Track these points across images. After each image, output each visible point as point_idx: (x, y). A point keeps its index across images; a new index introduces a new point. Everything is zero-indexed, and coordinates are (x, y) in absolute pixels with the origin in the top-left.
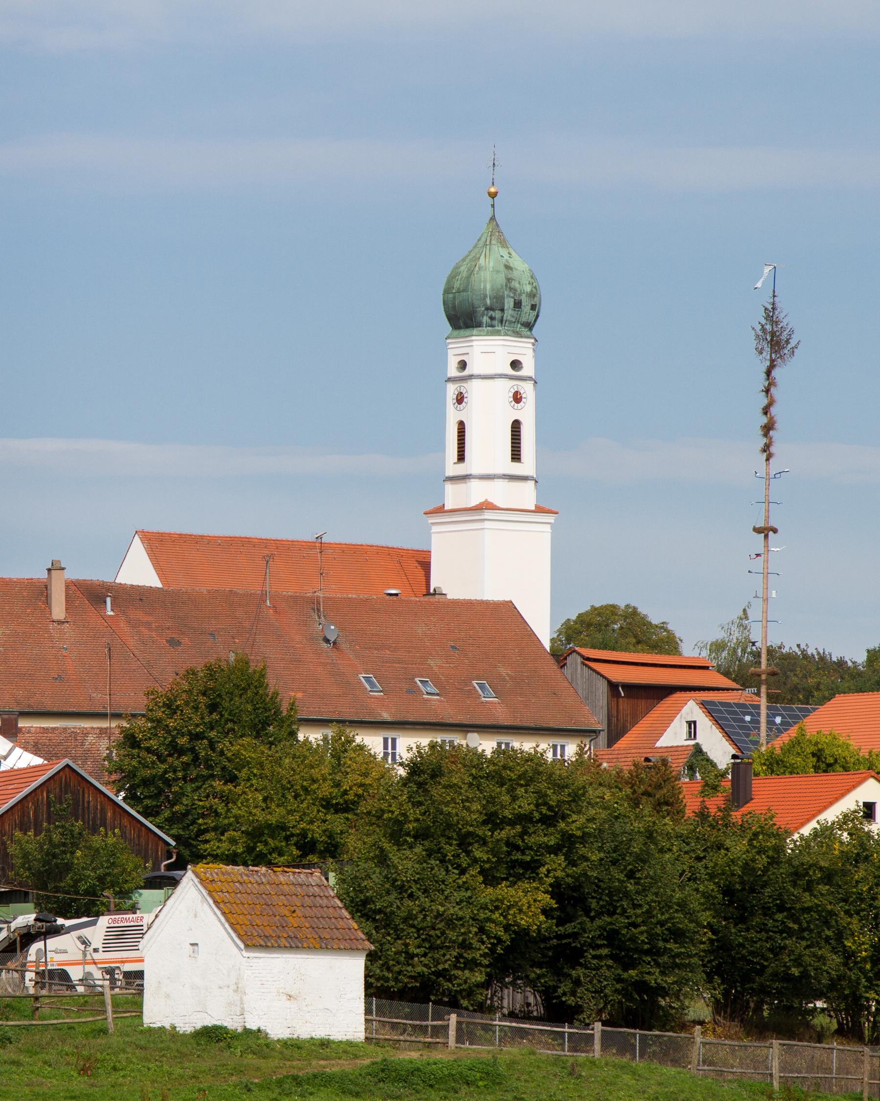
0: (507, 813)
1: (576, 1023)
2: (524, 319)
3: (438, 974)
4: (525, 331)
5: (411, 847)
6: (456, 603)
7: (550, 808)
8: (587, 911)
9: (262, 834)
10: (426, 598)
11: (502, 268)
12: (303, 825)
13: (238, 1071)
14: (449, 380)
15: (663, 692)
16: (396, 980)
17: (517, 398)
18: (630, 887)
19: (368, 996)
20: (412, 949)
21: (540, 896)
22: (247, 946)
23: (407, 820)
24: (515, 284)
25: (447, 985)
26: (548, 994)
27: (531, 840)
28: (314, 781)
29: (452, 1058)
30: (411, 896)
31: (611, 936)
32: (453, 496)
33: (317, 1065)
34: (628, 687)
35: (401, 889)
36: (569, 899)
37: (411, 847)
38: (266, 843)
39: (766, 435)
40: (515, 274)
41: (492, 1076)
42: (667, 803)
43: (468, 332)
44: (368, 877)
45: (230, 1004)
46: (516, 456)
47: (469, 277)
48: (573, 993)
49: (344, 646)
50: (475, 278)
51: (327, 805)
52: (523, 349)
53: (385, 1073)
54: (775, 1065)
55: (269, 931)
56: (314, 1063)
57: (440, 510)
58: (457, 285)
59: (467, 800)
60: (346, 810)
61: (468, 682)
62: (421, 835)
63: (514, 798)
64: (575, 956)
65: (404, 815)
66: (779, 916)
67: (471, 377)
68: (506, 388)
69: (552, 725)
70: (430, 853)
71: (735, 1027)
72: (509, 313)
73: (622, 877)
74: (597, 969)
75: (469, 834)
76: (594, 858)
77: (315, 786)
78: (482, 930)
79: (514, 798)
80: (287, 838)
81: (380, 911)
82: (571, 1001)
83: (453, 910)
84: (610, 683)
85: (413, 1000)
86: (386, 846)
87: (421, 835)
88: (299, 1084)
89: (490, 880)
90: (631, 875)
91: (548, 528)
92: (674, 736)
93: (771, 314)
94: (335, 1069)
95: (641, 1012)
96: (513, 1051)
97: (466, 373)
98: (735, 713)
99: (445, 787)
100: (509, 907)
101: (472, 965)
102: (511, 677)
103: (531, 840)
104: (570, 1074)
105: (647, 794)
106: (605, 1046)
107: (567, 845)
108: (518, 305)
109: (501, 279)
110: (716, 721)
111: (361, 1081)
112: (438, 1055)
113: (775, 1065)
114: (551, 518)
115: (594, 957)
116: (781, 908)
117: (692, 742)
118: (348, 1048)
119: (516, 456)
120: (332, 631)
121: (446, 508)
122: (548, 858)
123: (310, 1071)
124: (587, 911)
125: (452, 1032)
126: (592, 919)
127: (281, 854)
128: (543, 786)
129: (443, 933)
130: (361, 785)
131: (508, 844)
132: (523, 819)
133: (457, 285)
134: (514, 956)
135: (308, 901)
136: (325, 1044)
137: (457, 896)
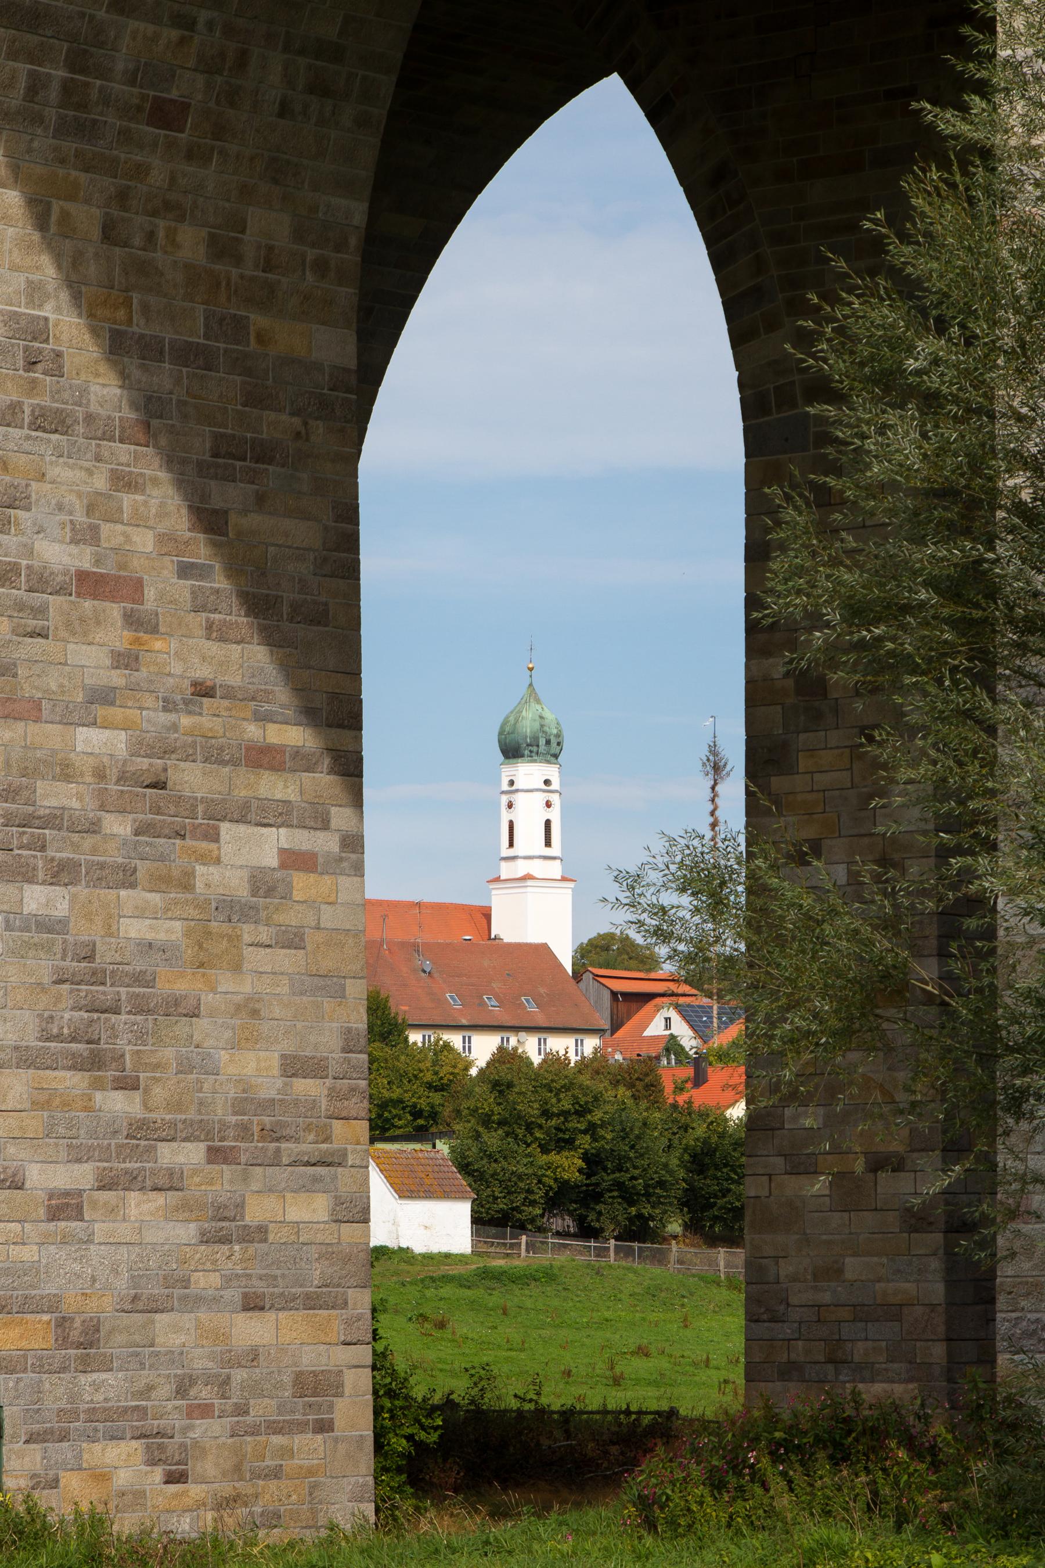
0: (555, 1110)
1: (601, 1239)
2: (552, 752)
3: (513, 1209)
4: (553, 759)
5: (495, 1131)
6: (509, 945)
7: (581, 1106)
8: (605, 1169)
9: (387, 1106)
10: (490, 942)
11: (537, 718)
12: (414, 1100)
13: (397, 1273)
14: (503, 792)
15: (648, 997)
16: (487, 1213)
17: (548, 805)
18: (632, 1155)
19: (472, 1223)
20: (496, 1194)
21: (576, 1161)
22: (400, 1197)
23: (493, 1114)
24: (546, 729)
25: (519, 1216)
26: (581, 1221)
27: (570, 1125)
28: (421, 1071)
29: (525, 1264)
30: (496, 1161)
31: (619, 1185)
32: (506, 870)
33: (445, 1269)
34: (625, 995)
35: (490, 1156)
36: (593, 1162)
37: (495, 1131)
38: (390, 1112)
39: (713, 829)
40: (546, 722)
41: (549, 1276)
42: (652, 1085)
43: (515, 760)
44: (469, 1149)
45: (389, 1232)
46: (548, 843)
47: (515, 724)
48: (598, 1220)
49: (436, 975)
50: (519, 725)
51: (430, 1086)
52: (552, 772)
53: (487, 1275)
54: (722, 1264)
55: (413, 1188)
56: (442, 1268)
57: (497, 880)
58: (507, 729)
59: (531, 1101)
60: (442, 1090)
61: (518, 998)
62: (501, 1123)
63: (559, 1100)
64: (597, 1196)
65: (492, 1111)
66: (725, 1170)
67: (517, 791)
68: (541, 798)
69: (574, 1026)
70: (507, 1134)
71: (697, 1239)
72: (542, 748)
73: (627, 1148)
74: (612, 1204)
75: (532, 1122)
76: (608, 1137)
77: (421, 1075)
78: (540, 1182)
79: (559, 1100)
80: (404, 1108)
81: (477, 1170)
82: (597, 1225)
83: (522, 1170)
84: (612, 991)
85: (497, 1226)
86: (481, 1129)
87: (501, 1123)
88: (434, 1281)
89: (545, 1150)
90: (632, 1147)
91: (570, 891)
92: (655, 1028)
93: (713, 750)
94: (455, 1272)
95: (639, 1232)
96: (562, 1258)
97: (514, 788)
98: (697, 1012)
99: (517, 1093)
100: (557, 1167)
101: (533, 1203)
102: (547, 994)
103: (570, 1125)
104: (597, 1273)
105: (638, 1079)
106: (616, 1253)
107: (591, 1129)
108: (548, 742)
109: (537, 726)
110: (684, 1017)
111: (471, 1279)
112: (516, 1262)
113: (722, 1264)
114: (572, 885)
115: (610, 1197)
116: (726, 1165)
117: (668, 1033)
118: (461, 1258)
119: (548, 843)
120: (428, 965)
121: (502, 878)
122: (580, 1136)
123: (441, 1273)
124: (605, 1169)
125: (523, 1247)
126: (608, 1174)
127: (400, 1119)
128: (576, 1092)
129: (516, 1184)
130: (452, 1074)
131: (556, 1128)
132: (565, 1114)
133: (507, 729)
134: (559, 1197)
135: (436, 1169)
136: (447, 1256)
137: (525, 1160)
